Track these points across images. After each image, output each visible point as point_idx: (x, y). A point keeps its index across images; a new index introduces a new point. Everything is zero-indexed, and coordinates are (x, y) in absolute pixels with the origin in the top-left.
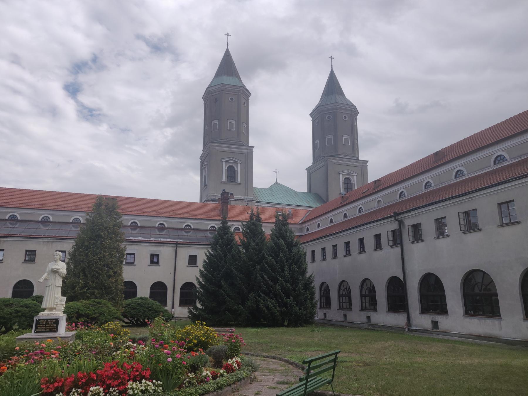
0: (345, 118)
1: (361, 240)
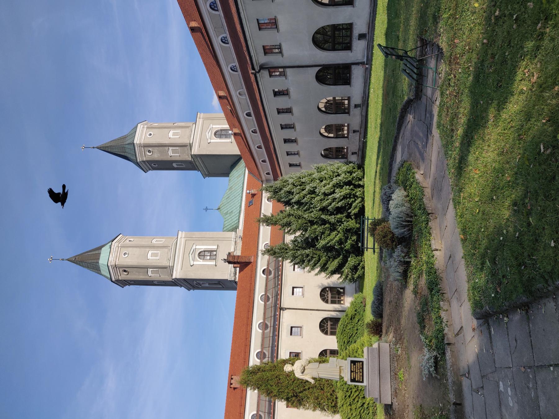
0: (151, 134)
1: (279, 112)
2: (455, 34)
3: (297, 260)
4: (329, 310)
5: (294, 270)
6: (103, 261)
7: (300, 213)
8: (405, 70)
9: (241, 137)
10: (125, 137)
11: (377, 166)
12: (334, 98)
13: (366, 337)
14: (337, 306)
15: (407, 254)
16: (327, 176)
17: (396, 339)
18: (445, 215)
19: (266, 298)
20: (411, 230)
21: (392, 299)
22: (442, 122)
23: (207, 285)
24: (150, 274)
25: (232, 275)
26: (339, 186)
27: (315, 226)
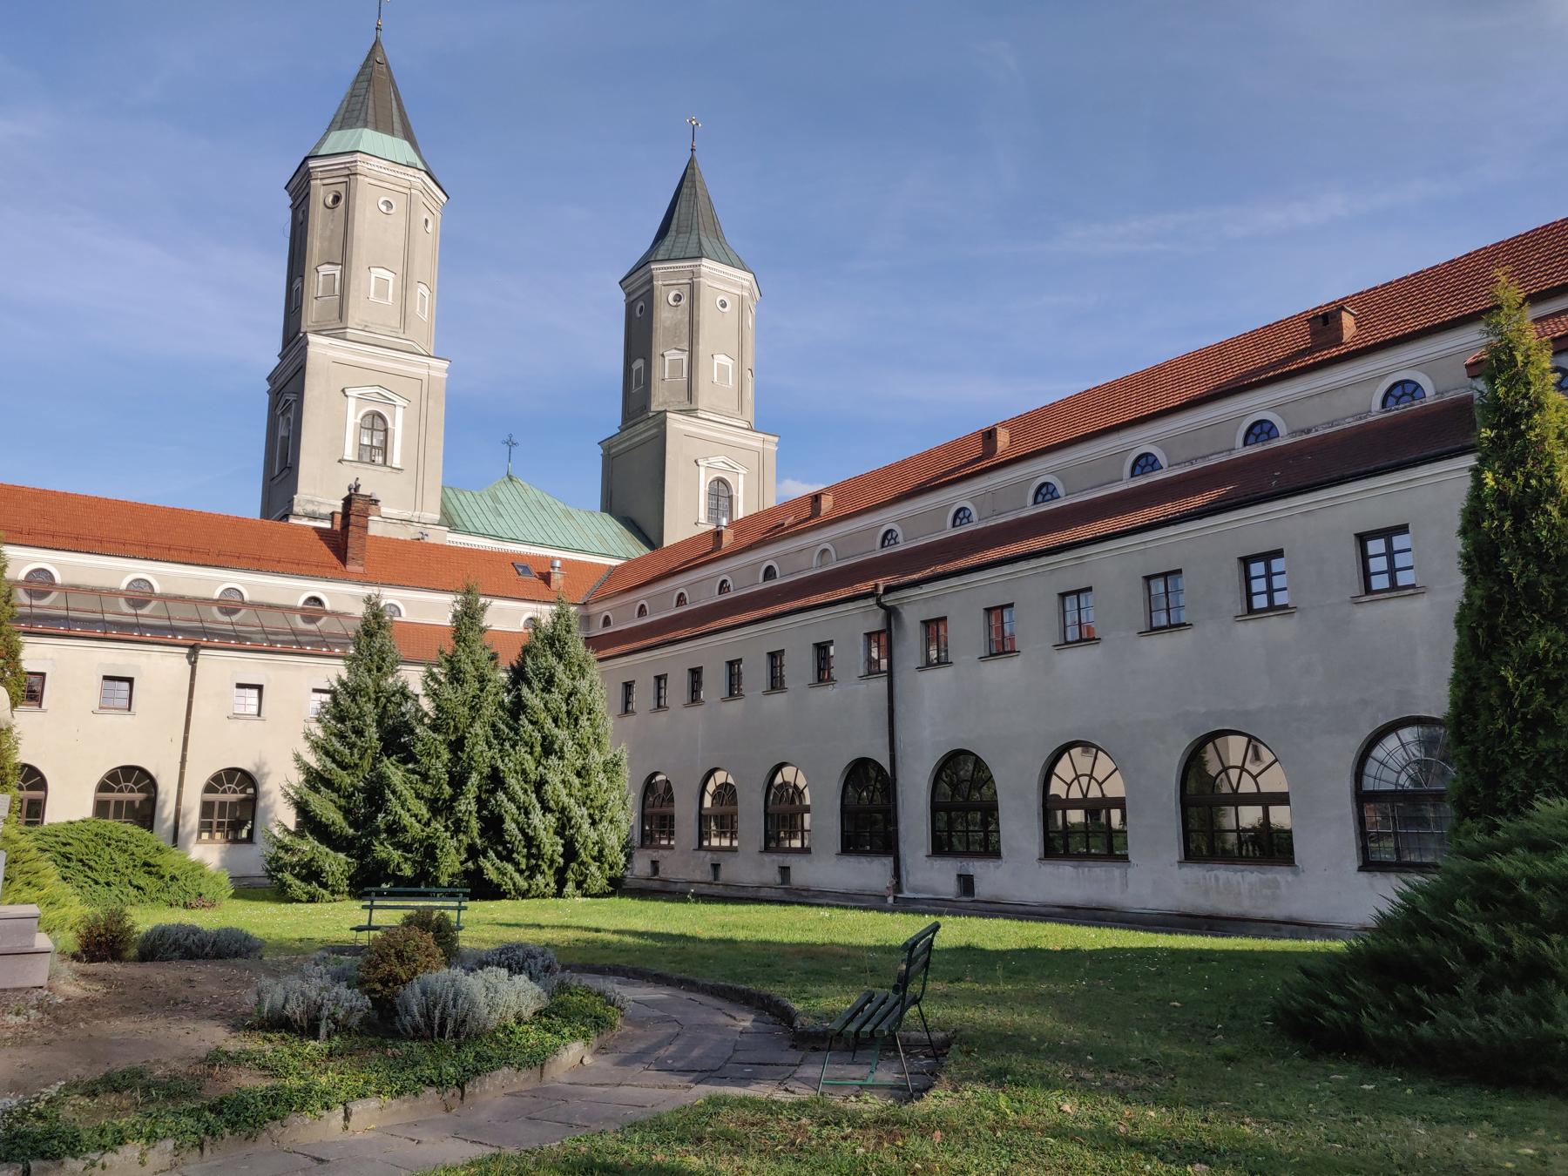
0: (724, 305)
1: (775, 657)
2: (956, 1131)
3: (345, 701)
4: (183, 795)
5: (315, 691)
6: (368, 138)
7: (488, 711)
8: (870, 1001)
9: (710, 549)
10: (718, 234)
11: (615, 932)
12: (807, 809)
13: (77, 909)
14: (193, 818)
15: (341, 1028)
16: (592, 789)
17: (60, 1006)
18: (455, 1136)
19: (230, 604)
20: (417, 1034)
21: (198, 989)
22: (725, 1109)
23: (282, 432)
24: (326, 269)
25: (310, 508)
26: (564, 825)
27: (446, 756)
